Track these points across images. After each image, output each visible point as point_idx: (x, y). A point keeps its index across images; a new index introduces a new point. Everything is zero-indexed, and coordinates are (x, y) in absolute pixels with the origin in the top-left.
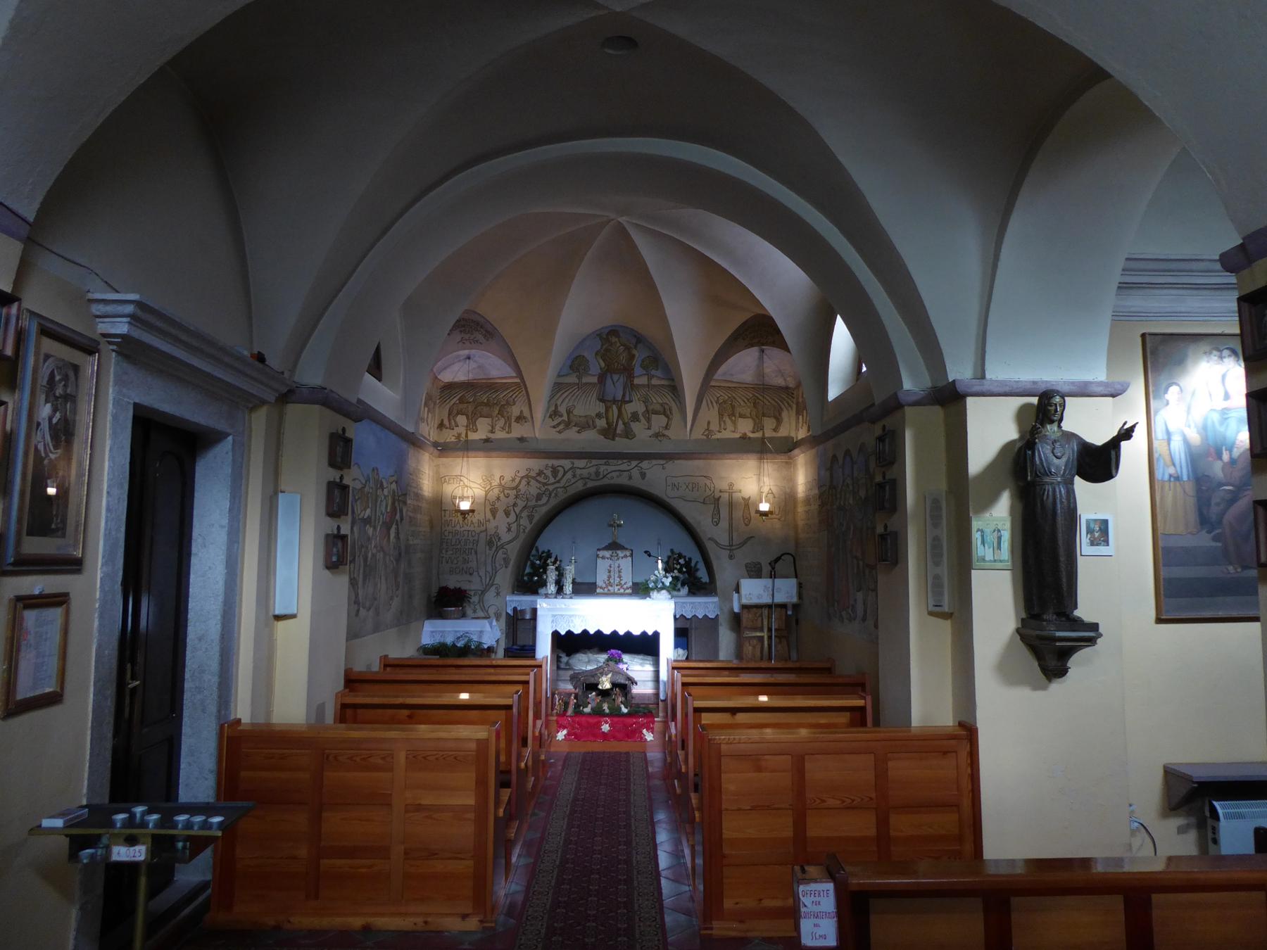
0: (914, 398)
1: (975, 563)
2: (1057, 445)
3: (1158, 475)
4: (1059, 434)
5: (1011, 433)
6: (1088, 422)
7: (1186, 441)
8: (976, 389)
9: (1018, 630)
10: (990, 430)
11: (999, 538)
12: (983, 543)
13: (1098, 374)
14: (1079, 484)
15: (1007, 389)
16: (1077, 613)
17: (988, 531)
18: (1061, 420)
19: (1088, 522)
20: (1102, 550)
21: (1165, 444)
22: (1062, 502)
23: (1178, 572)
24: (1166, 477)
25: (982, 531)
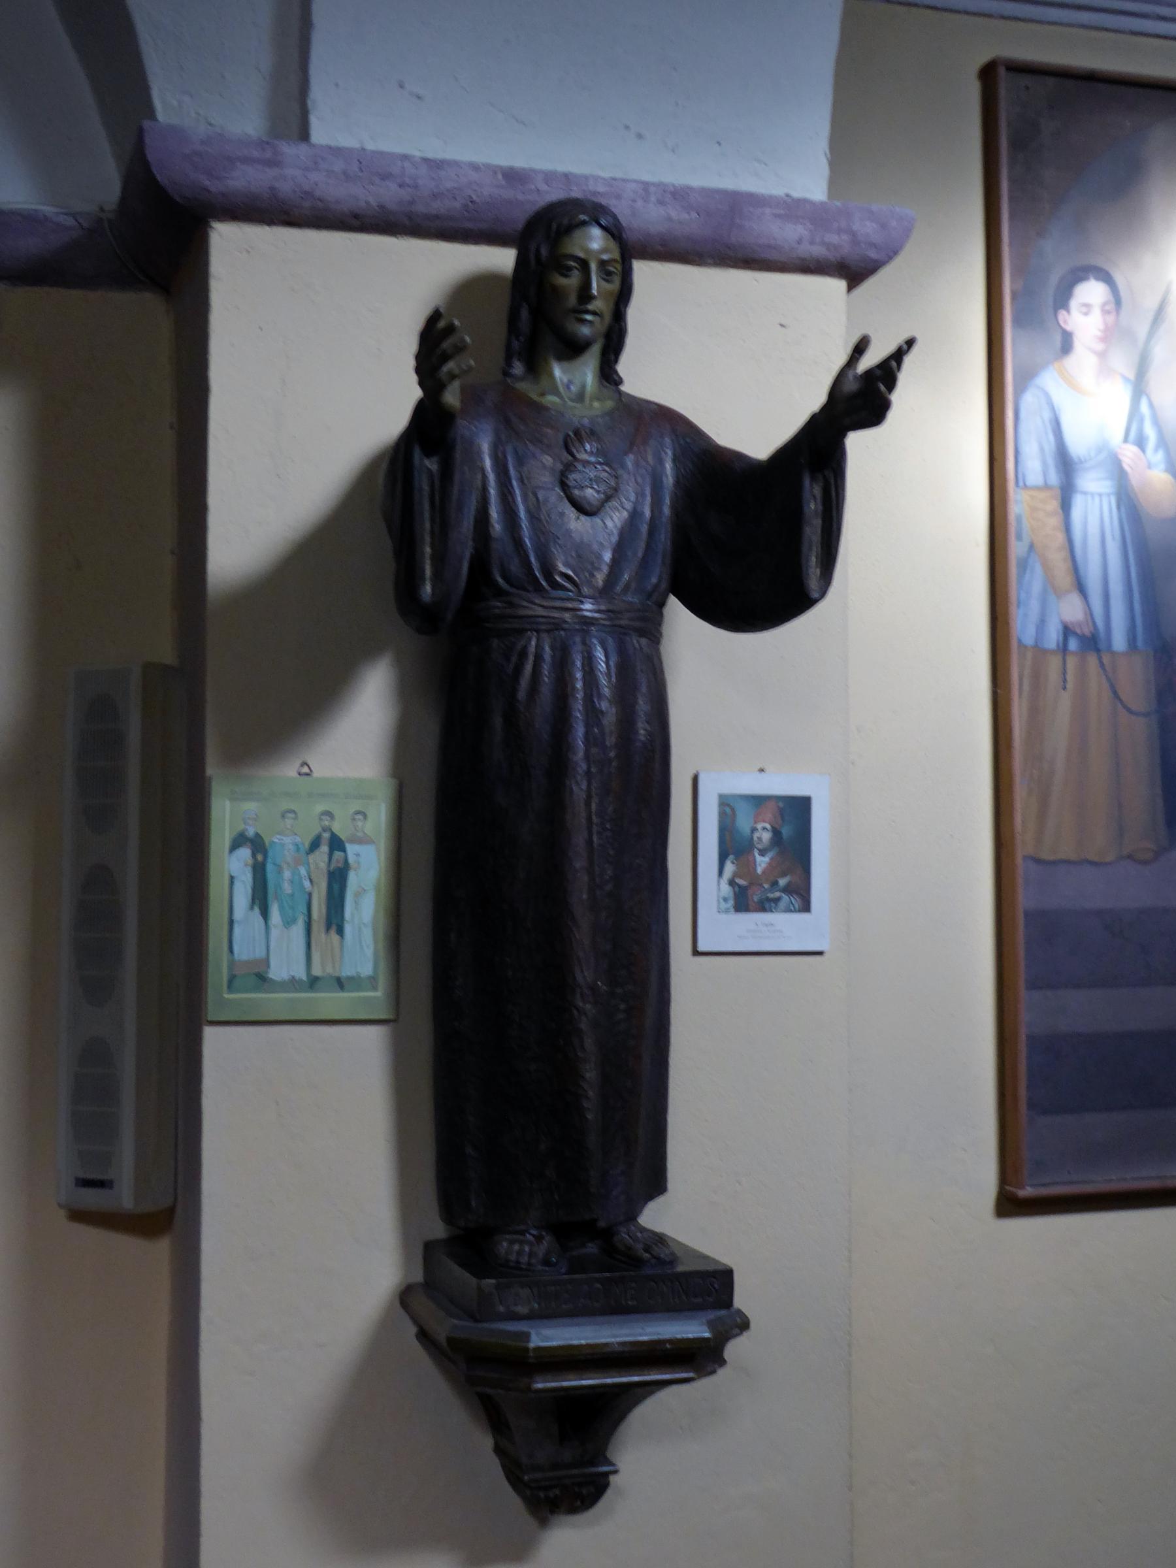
0: (29, 246)
1: (219, 993)
2: (586, 452)
3: (1024, 626)
4: (597, 408)
5: (387, 403)
6: (723, 363)
7: (1129, 502)
8: (246, 179)
9: (405, 1296)
10: (307, 383)
11: (338, 878)
12: (261, 898)
13: (791, 166)
14: (686, 635)
15: (388, 195)
16: (655, 1217)
17: (285, 844)
18: (614, 341)
19: (727, 805)
20: (781, 928)
21: (1054, 505)
22: (593, 714)
23: (1086, 1011)
24: (1053, 637)
25: (258, 845)
